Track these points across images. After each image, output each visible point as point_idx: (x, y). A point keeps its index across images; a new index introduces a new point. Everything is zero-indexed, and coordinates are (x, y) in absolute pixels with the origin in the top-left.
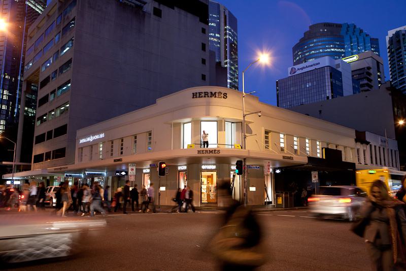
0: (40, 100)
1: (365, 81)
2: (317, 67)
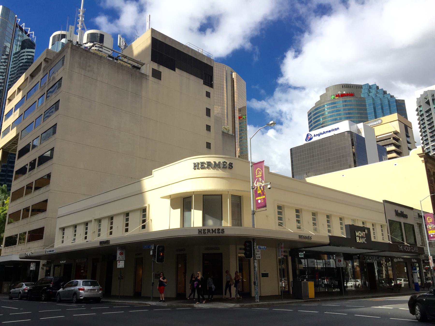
0: (16, 172)
2: (336, 132)
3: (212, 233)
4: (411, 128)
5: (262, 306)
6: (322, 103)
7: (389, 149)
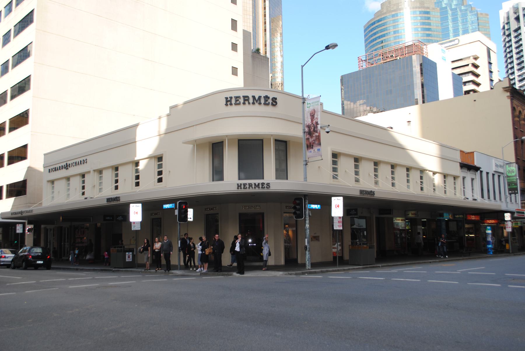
1: (470, 77)
3: (255, 188)
6: (384, 14)
7: (465, 79)
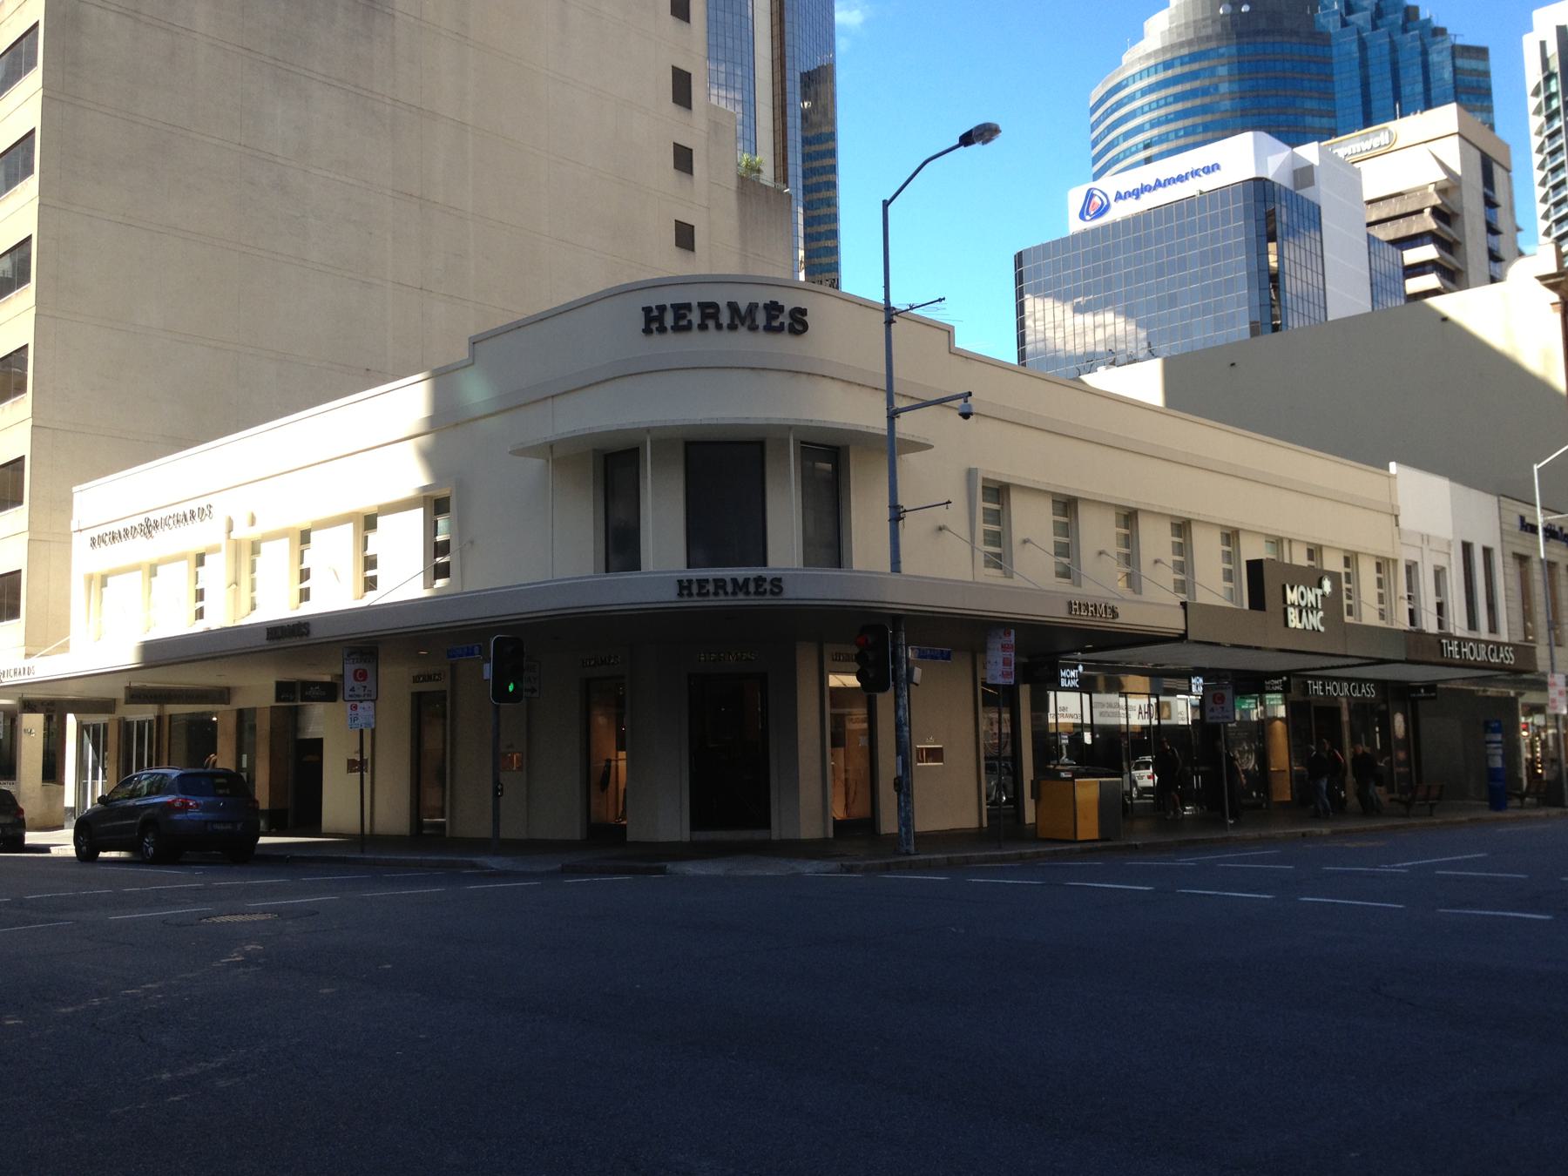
3: (734, 593)
4: (1508, 171)
5: (929, 867)
